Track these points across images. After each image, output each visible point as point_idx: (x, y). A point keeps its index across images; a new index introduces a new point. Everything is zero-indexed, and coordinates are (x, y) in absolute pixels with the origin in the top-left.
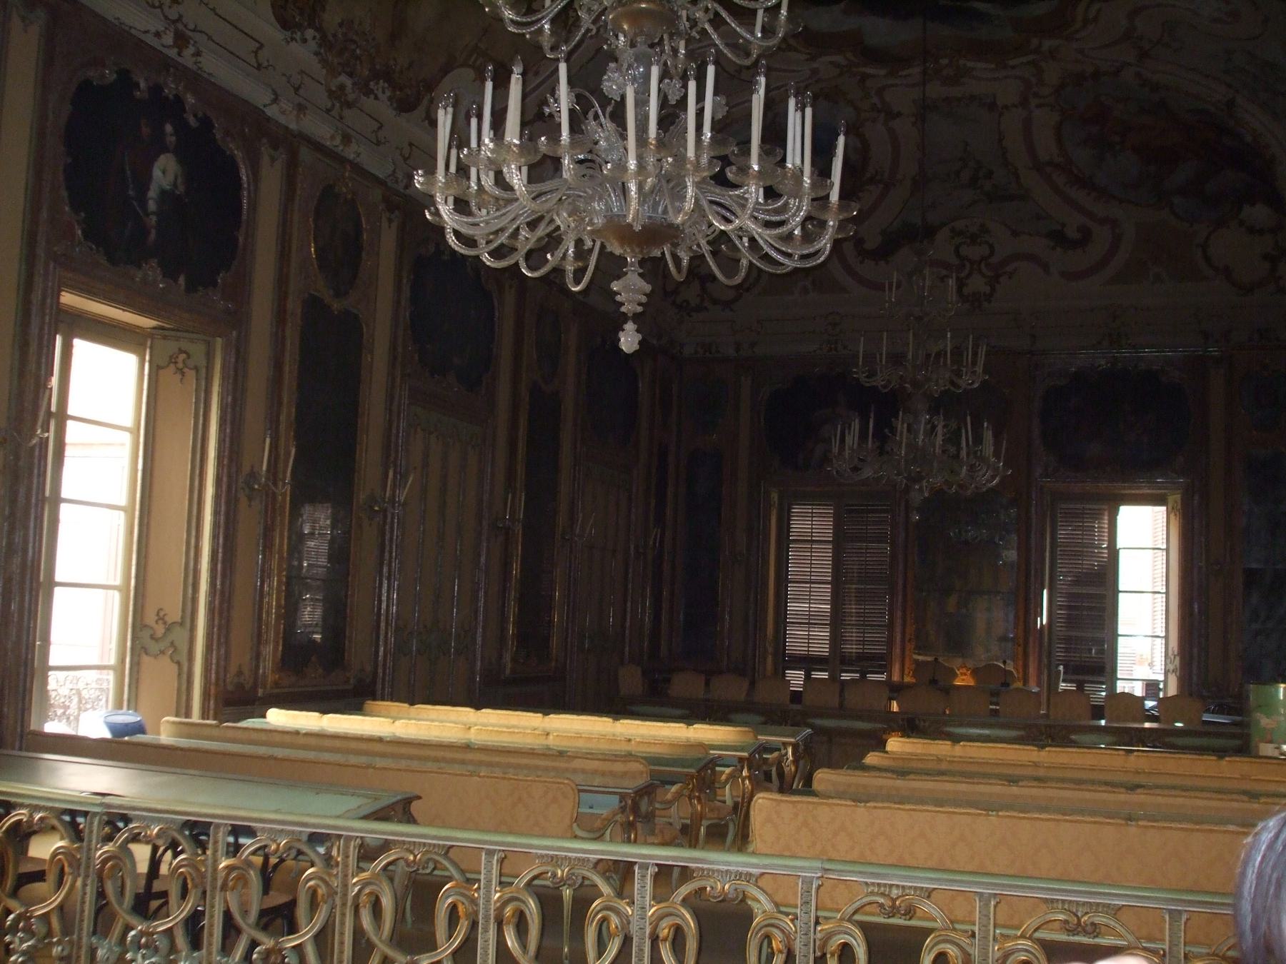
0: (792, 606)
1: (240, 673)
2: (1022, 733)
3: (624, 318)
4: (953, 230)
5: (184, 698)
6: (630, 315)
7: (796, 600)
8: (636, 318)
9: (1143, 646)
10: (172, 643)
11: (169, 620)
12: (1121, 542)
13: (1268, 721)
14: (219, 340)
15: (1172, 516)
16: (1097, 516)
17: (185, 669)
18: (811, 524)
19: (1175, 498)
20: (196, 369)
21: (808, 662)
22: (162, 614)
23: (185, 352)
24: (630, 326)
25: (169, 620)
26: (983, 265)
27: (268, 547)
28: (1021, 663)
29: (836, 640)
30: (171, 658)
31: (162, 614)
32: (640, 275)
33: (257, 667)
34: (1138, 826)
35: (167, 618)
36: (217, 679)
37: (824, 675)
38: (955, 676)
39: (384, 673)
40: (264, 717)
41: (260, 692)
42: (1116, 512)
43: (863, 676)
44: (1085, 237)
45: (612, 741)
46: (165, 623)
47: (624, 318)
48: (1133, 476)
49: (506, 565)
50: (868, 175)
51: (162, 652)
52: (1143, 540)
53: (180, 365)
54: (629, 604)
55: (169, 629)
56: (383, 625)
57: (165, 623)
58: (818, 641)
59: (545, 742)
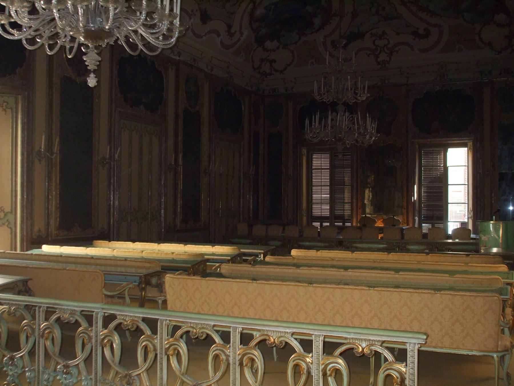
0: (315, 196)
1: (39, 231)
2: (327, 244)
3: (90, 72)
4: (371, 34)
5: (14, 242)
6: (92, 70)
7: (316, 193)
8: (95, 71)
9: (458, 209)
10: (8, 220)
11: (6, 211)
12: (448, 165)
13: (485, 237)
14: (20, 96)
15: (470, 152)
16: (439, 153)
17: (14, 230)
18: (321, 161)
19: (470, 144)
20: (12, 109)
21: (321, 219)
22: (2, 208)
23: (6, 102)
24: (92, 75)
25: (6, 211)
26: (385, 48)
27: (50, 180)
28: (405, 216)
29: (332, 209)
30: (7, 226)
31: (2, 208)
32: (97, 54)
33: (48, 229)
34: (313, 287)
35: (5, 210)
36: (27, 233)
37: (328, 224)
38: (376, 222)
39: (114, 229)
40: (41, 248)
41: (50, 238)
42: (447, 150)
43: (344, 224)
44: (428, 33)
45: (166, 254)
46: (4, 212)
47: (90, 72)
48: (454, 135)
49: (176, 185)
50: (333, 13)
51: (4, 224)
52: (458, 161)
53: (4, 108)
54: (242, 200)
55: (6, 214)
56: (112, 210)
57: (4, 212)
58: (324, 210)
59: (141, 255)
